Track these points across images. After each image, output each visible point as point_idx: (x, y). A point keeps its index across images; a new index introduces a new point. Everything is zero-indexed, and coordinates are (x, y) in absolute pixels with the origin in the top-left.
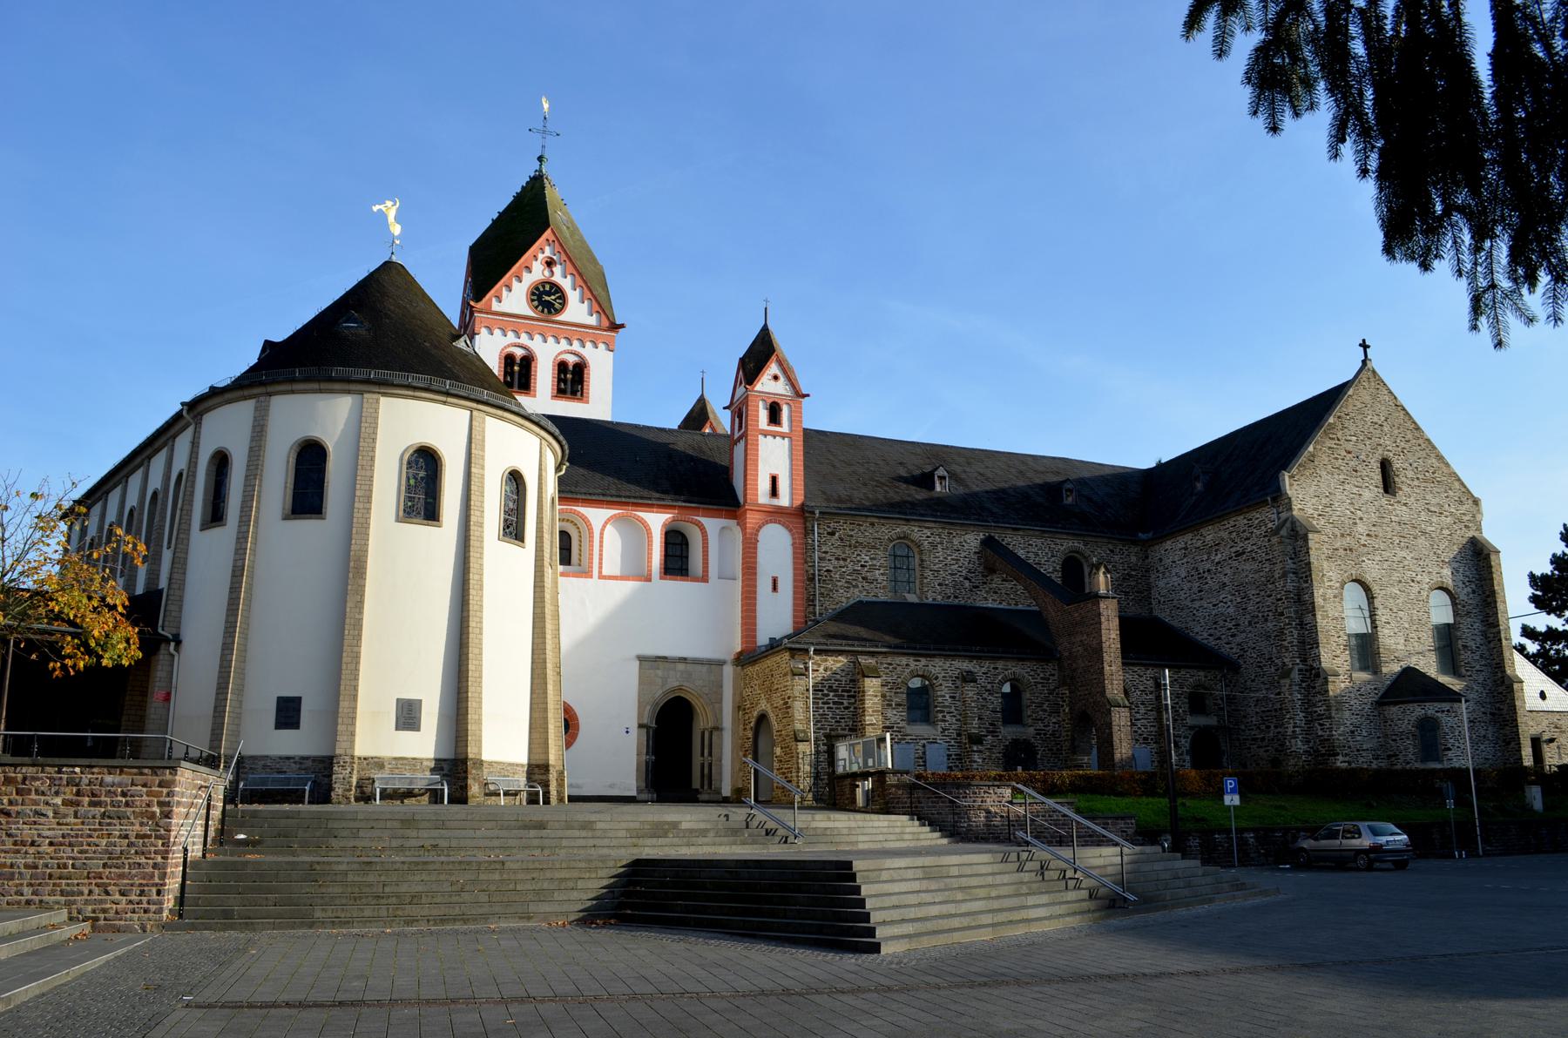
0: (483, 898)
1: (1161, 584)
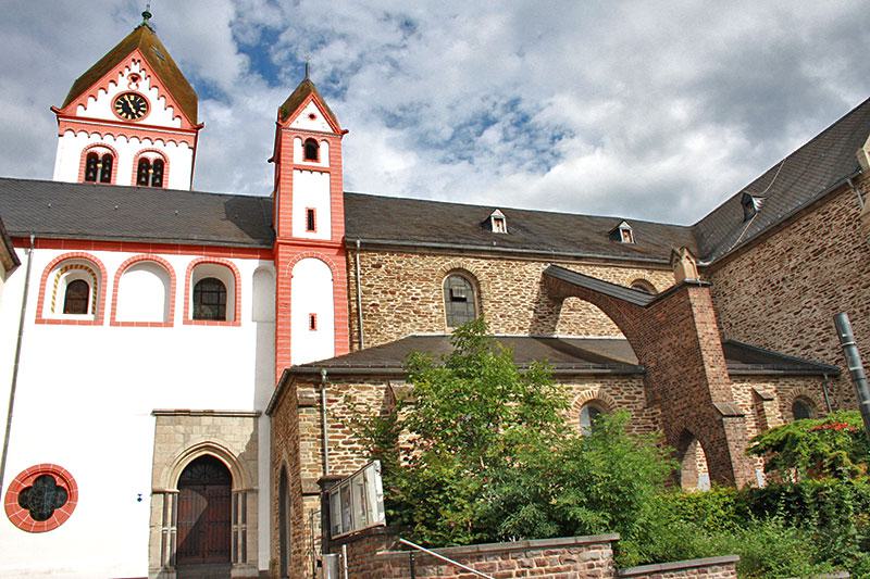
1: (730, 306)
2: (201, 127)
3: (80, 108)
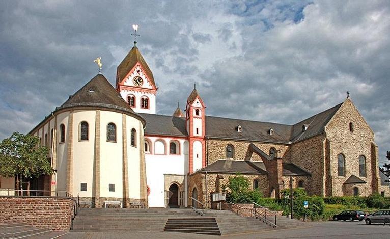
1: (294, 155)
2: (158, 89)
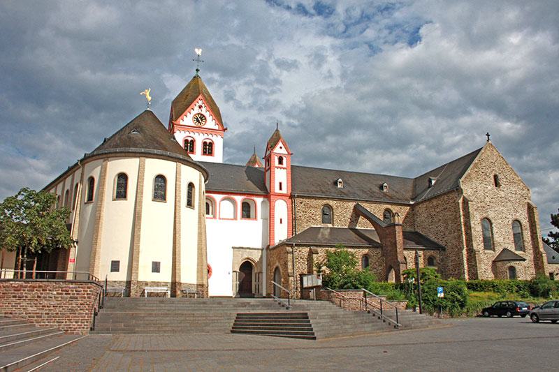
0: (188, 325)
3: (181, 121)
